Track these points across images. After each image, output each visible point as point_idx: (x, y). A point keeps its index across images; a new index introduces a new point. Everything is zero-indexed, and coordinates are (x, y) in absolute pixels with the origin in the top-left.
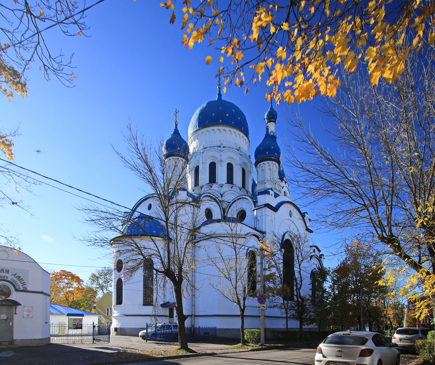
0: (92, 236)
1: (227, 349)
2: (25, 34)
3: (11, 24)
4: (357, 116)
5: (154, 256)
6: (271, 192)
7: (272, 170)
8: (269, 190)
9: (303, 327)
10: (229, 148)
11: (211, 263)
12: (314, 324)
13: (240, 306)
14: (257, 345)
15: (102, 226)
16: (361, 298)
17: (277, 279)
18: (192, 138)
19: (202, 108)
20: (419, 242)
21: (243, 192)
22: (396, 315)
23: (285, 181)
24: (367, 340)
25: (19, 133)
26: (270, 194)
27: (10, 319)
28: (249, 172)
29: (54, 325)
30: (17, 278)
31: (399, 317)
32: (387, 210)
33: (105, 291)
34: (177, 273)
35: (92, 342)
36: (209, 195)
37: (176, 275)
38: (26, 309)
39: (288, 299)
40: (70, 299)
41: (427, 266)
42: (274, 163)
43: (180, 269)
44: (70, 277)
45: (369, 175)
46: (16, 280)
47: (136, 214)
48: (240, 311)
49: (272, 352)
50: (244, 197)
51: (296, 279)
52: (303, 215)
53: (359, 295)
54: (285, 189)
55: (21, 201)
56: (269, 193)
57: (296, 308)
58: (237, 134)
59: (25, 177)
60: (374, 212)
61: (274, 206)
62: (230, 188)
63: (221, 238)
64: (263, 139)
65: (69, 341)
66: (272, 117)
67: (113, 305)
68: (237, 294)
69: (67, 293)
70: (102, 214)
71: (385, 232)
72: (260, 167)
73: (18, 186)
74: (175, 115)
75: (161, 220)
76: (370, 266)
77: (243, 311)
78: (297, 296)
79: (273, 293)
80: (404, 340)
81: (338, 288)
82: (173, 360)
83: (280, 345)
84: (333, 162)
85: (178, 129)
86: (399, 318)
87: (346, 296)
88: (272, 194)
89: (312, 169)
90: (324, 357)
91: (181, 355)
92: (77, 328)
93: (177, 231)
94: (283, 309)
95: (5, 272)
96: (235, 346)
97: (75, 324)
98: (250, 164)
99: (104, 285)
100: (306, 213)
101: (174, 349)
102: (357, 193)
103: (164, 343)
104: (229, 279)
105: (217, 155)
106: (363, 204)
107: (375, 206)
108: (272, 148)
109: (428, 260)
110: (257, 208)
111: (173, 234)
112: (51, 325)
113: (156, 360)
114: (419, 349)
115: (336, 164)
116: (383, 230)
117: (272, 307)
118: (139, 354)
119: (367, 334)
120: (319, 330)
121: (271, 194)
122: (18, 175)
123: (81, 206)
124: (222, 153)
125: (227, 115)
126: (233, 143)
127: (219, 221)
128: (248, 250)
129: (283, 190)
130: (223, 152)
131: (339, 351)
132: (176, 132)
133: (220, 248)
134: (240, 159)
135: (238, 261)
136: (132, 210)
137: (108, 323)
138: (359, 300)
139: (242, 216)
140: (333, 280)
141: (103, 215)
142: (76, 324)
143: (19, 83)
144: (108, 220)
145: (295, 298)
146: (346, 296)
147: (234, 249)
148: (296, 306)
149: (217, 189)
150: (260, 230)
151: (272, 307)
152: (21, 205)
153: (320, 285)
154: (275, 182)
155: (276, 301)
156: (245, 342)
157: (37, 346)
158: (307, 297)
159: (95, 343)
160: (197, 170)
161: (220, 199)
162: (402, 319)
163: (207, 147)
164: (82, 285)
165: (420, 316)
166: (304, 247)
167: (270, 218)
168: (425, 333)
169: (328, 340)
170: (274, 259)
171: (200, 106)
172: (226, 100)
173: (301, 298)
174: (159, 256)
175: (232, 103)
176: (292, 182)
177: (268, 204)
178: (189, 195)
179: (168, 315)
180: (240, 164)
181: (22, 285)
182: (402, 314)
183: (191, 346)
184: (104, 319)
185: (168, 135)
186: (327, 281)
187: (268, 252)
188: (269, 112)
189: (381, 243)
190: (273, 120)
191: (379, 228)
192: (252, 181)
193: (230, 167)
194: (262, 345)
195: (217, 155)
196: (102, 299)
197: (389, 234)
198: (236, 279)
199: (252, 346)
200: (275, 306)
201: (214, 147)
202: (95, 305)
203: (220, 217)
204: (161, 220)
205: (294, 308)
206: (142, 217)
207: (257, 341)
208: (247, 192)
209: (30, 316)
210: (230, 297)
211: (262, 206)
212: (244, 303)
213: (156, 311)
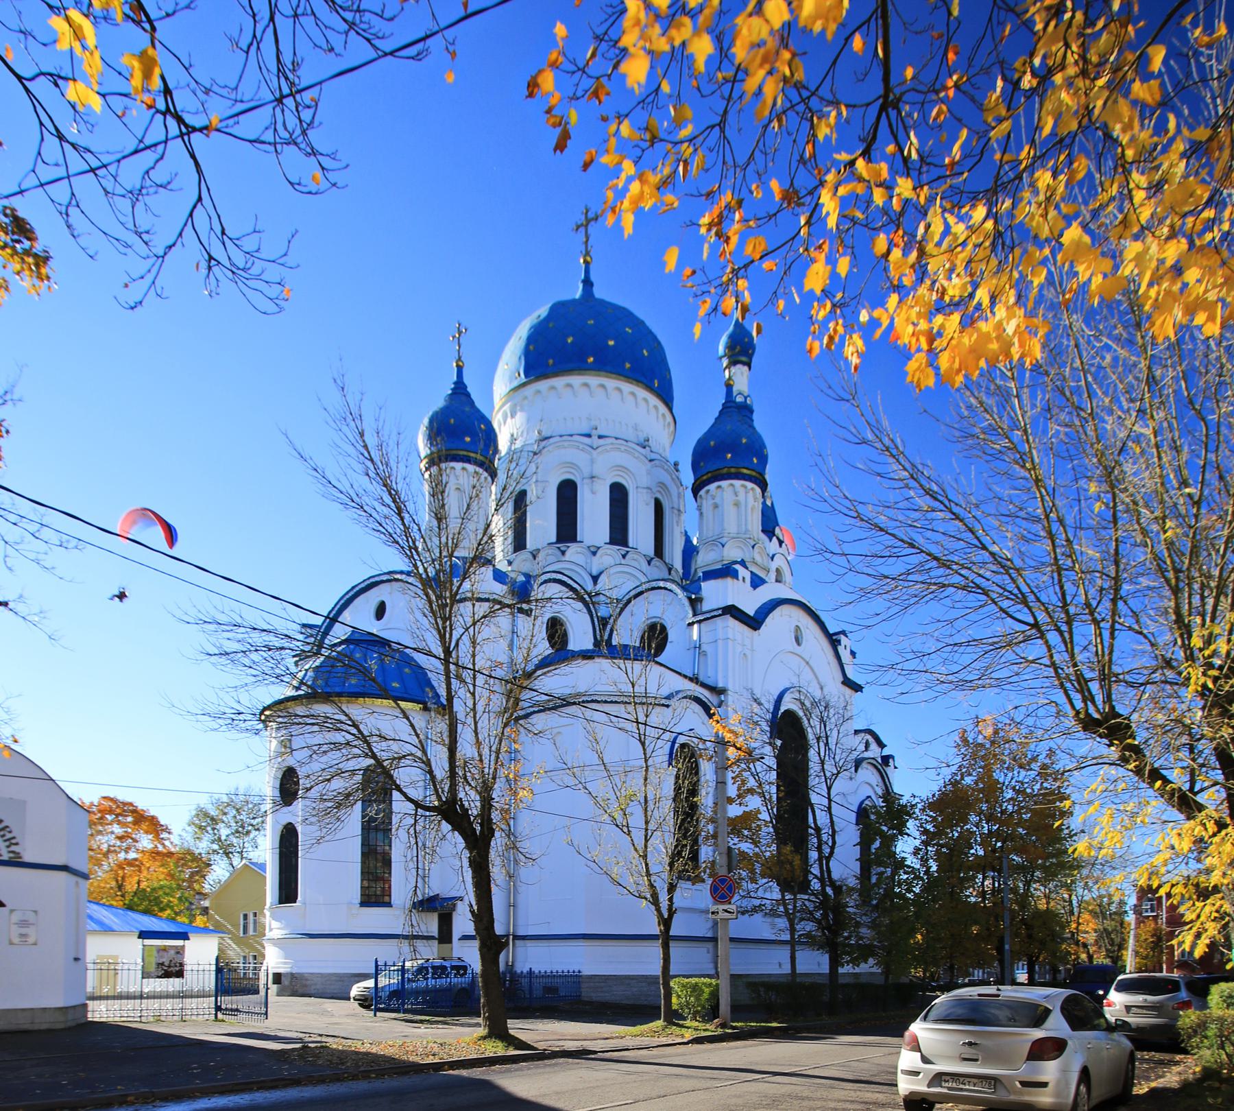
0: (229, 702)
1: (622, 1038)
2: (153, 168)
3: (90, 127)
4: (1013, 374)
5: (408, 762)
6: (742, 572)
7: (743, 508)
8: (737, 567)
9: (841, 970)
10: (617, 439)
11: (572, 781)
12: (871, 961)
13: (658, 910)
14: (708, 1026)
15: (254, 672)
16: (1005, 883)
17: (764, 829)
18: (507, 407)
19: (535, 321)
20: (1190, 734)
21: (657, 570)
22: (1104, 934)
23: (778, 538)
24: (1047, 1012)
25: (15, 397)
26: (737, 579)
28: (676, 512)
31: (1112, 939)
32: (1099, 641)
33: (236, 861)
35: (213, 1017)
36: (559, 577)
37: (472, 818)
38: (15, 917)
39: (796, 890)
40: (131, 886)
41: (1212, 798)
42: (750, 485)
43: (487, 803)
44: (130, 819)
45: (1049, 541)
47: (339, 633)
48: (659, 925)
49: (755, 1045)
50: (661, 584)
51: (818, 830)
52: (833, 640)
53: (999, 875)
54: (779, 562)
55: (21, 596)
56: (735, 575)
57: (818, 915)
58: (651, 406)
59: (33, 528)
60: (1063, 646)
61: (750, 611)
62: (619, 559)
63: (594, 706)
64: (717, 414)
65: (144, 1013)
66: (741, 350)
67: (268, 905)
68: (648, 874)
69: (121, 866)
70: (255, 634)
71: (1093, 702)
72: (709, 497)
73: (10, 550)
74: (456, 340)
75: (429, 654)
76: (1029, 791)
77: (666, 923)
78: (821, 880)
79: (753, 871)
80: (1139, 1011)
81: (938, 853)
82: (470, 1071)
83: (775, 1025)
84: (946, 503)
85: (466, 380)
86: (1112, 943)
87: (962, 880)
89: (882, 520)
90: (925, 1060)
91: (491, 1055)
92: (167, 975)
93: (474, 686)
94: (780, 916)
96: (645, 1027)
97: (162, 964)
98: (678, 488)
99: (235, 841)
100: (843, 633)
101: (467, 1039)
102: (1016, 591)
103: (427, 1018)
104: (625, 830)
105: (581, 458)
106: (1031, 621)
107: (1064, 628)
108: (744, 441)
109: (1215, 784)
110: (701, 617)
111: (463, 697)
112: (90, 966)
113: (422, 1071)
114: (1190, 1037)
115: (956, 509)
116: (1088, 698)
117: (748, 911)
118: (367, 1054)
119: (1048, 996)
120: (887, 978)
122: (13, 518)
123: (193, 612)
125: (611, 343)
126: (620, 423)
127: (586, 655)
128: (674, 742)
129: (773, 566)
130: (600, 449)
131: (970, 1044)
132: (460, 389)
133: (599, 737)
134: (649, 473)
135: (651, 776)
136: (327, 617)
137: (245, 957)
138: (1000, 891)
139: (656, 638)
140: (925, 832)
141: (258, 639)
142: (166, 964)
143: (27, 252)
144: (270, 653)
145: (815, 885)
146: (962, 880)
147: (640, 740)
148: (817, 908)
149: (580, 559)
150: (710, 682)
151: (748, 911)
152: (20, 608)
153: (889, 847)
154: (753, 543)
155: (760, 894)
156: (674, 1018)
157: (49, 1031)
158: (852, 882)
159: (223, 1021)
160: (520, 501)
161: (589, 586)
162: (1122, 946)
163: (549, 435)
164: (167, 843)
165: (1194, 946)
166: (841, 735)
167: (739, 649)
168: (1200, 991)
169: (932, 1015)
170: (753, 770)
171: (529, 314)
172: (608, 299)
173: (832, 883)
174: (423, 762)
175: (624, 309)
176: (828, 555)
177: (733, 606)
178: (499, 576)
179: (436, 934)
180: (648, 488)
181: (8, 847)
182: (1122, 933)
183: (517, 1028)
184: (234, 946)
185: (438, 400)
186: (909, 835)
187: (739, 749)
188: (731, 337)
189: (1081, 735)
190: (744, 359)
191: (1077, 691)
192: (684, 538)
193: (619, 496)
194: (723, 1026)
195: (581, 458)
196: (226, 887)
197: (1104, 709)
198: (647, 830)
199: (693, 1027)
200: (755, 910)
201: (571, 435)
202: (206, 903)
203: (588, 645)
204: (429, 654)
205: (811, 913)
206: (362, 641)
207: (712, 1012)
208: (670, 570)
209: (31, 940)
210: (629, 881)
212: (671, 900)
213: (415, 923)
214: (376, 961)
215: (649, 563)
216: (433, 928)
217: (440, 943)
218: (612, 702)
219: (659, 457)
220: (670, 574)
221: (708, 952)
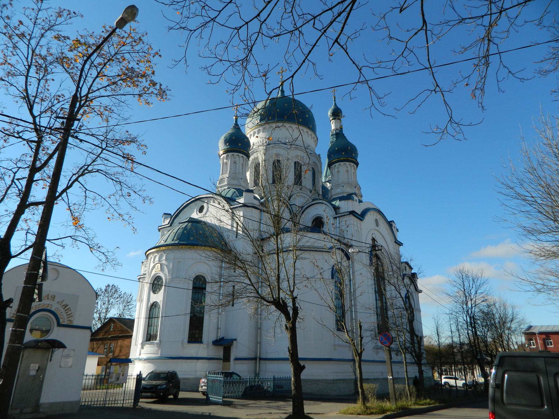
6: (355, 198)
8: (354, 196)
27: (42, 370)
28: (320, 172)
29: (88, 377)
30: (64, 307)
34: (290, 303)
42: (352, 164)
46: (62, 310)
56: (353, 200)
58: (309, 135)
88: (356, 200)
95: (50, 298)
121: (355, 200)
124: (289, 151)
132: (236, 125)
154: (355, 186)
167: (356, 228)
179: (222, 357)
185: (229, 130)
193: (298, 166)
211: (346, 214)
214: (140, 372)
215: (311, 192)
216: (220, 354)
217: (224, 361)
218: (319, 251)
219: (313, 152)
220: (319, 196)
221: (351, 367)
